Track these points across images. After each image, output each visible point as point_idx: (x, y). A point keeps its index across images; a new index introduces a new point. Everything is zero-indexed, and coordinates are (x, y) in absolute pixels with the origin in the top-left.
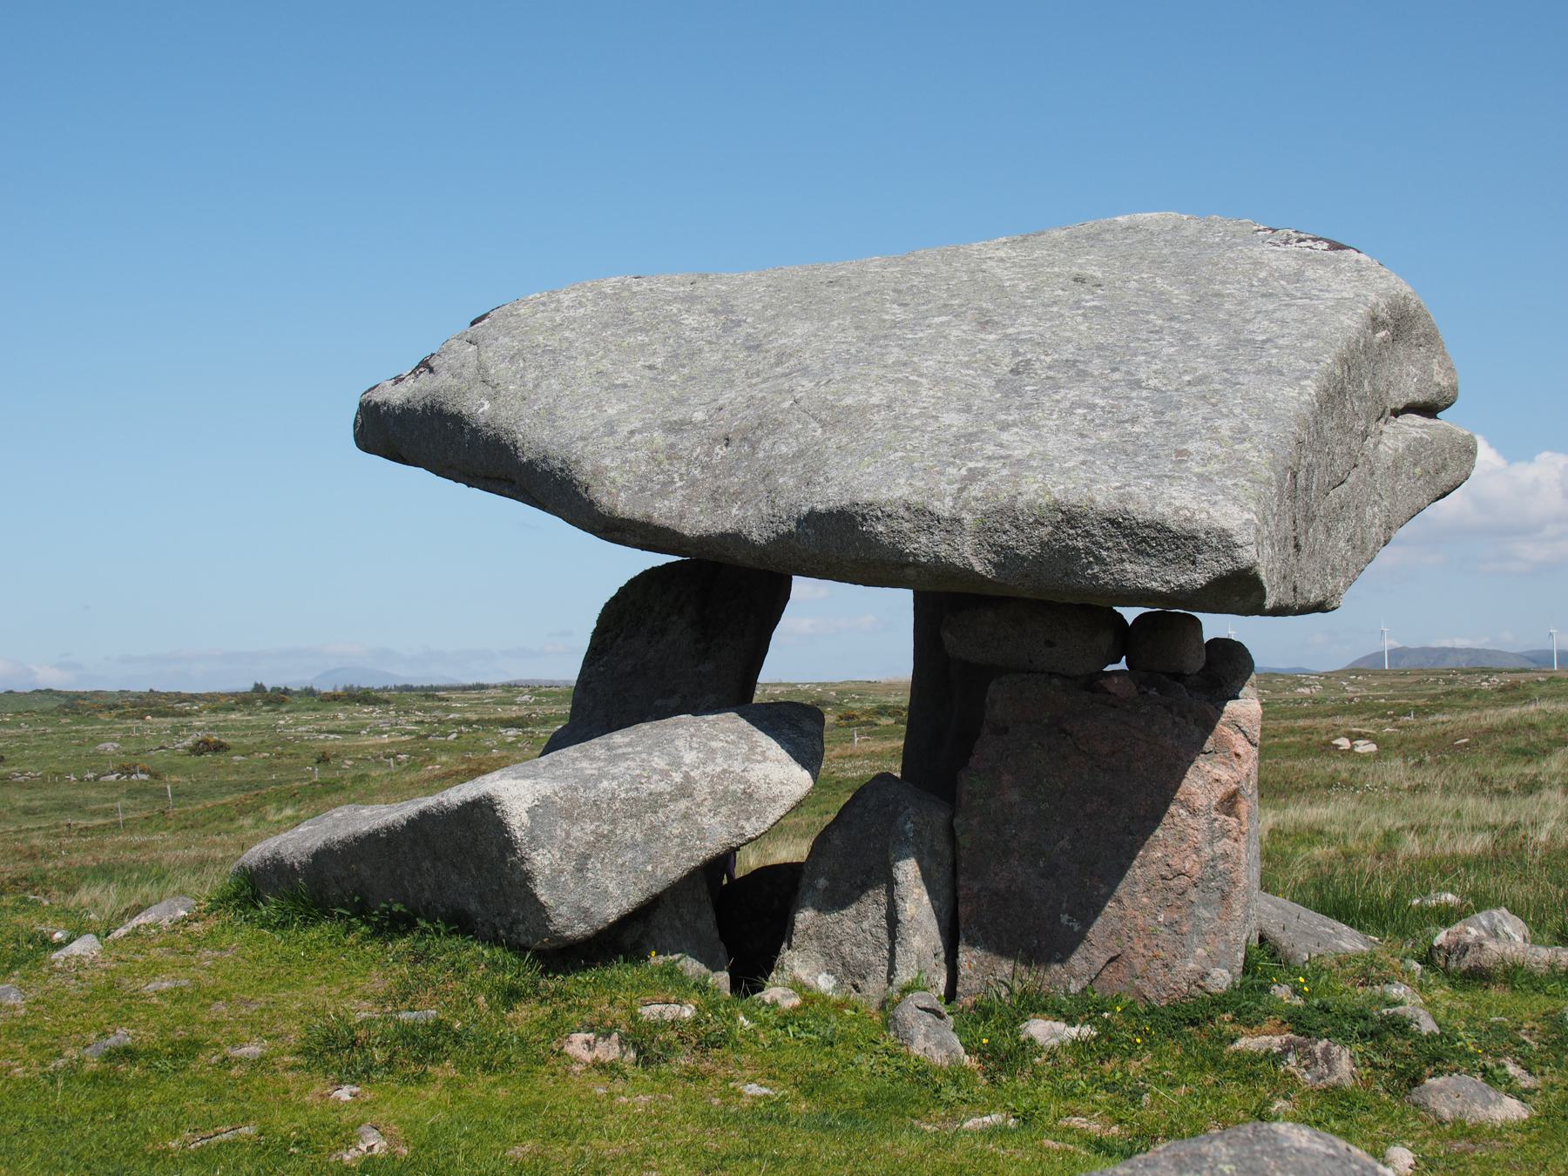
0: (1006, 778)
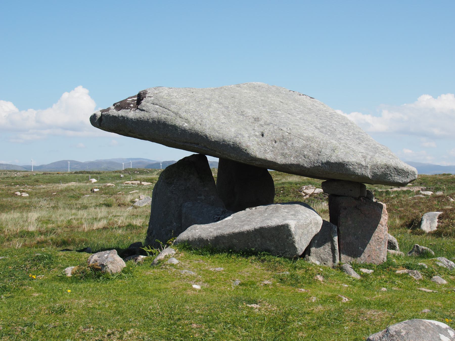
0: (349, 219)
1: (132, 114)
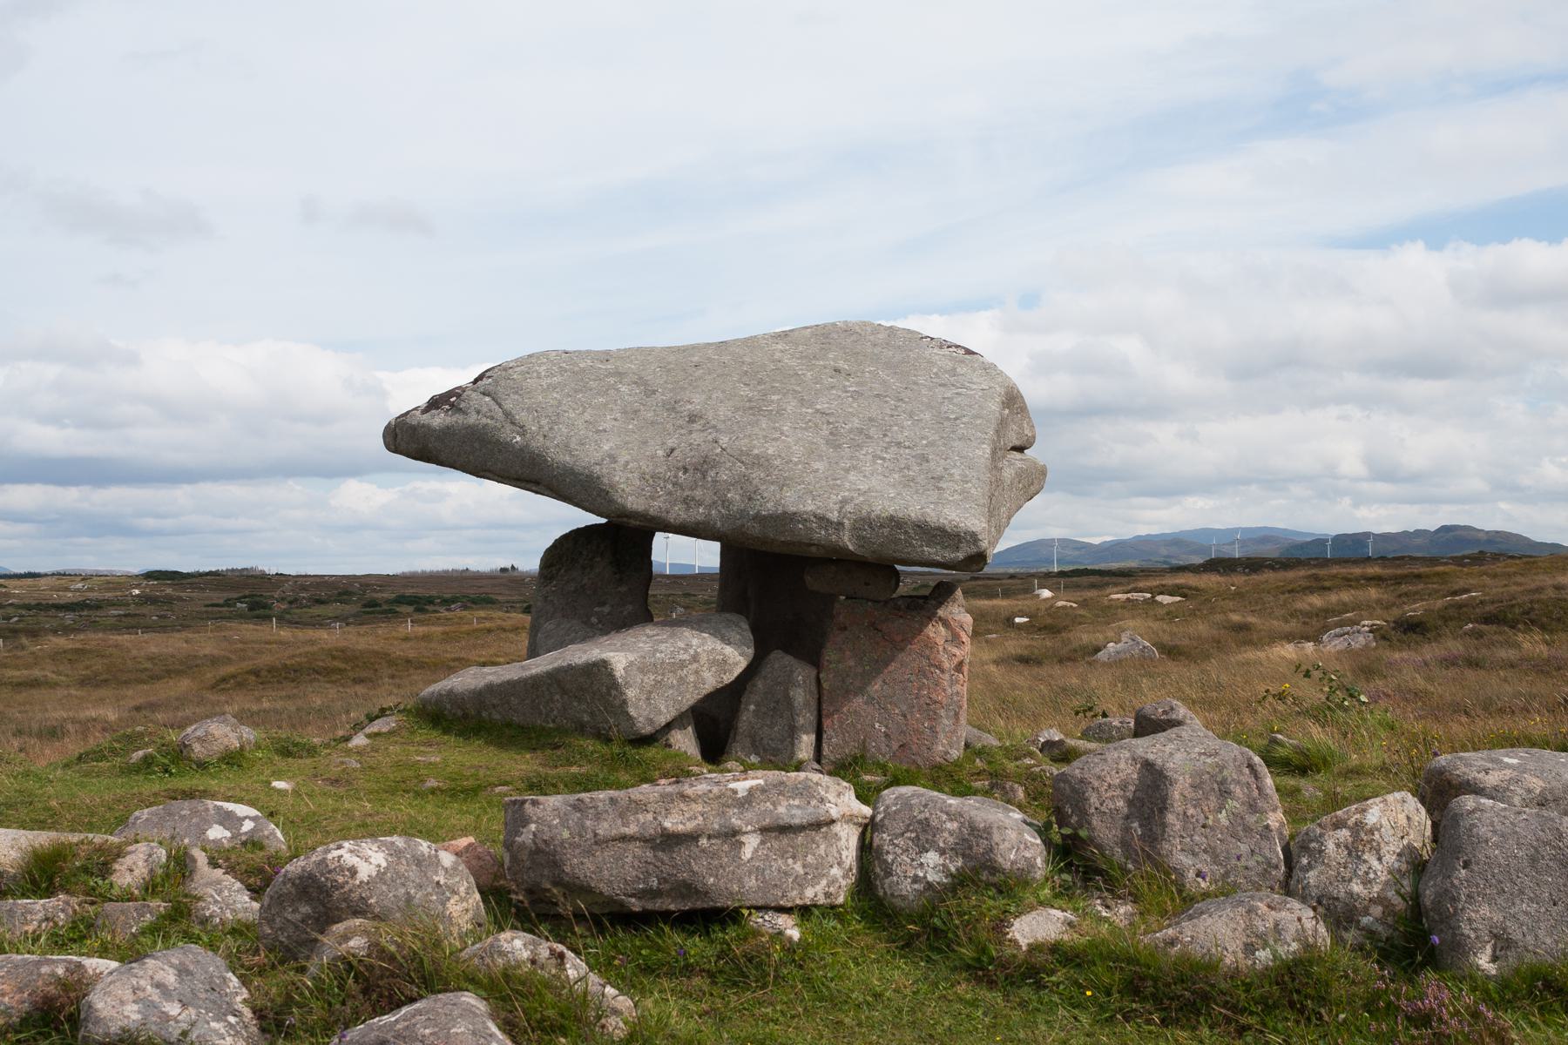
1: (438, 419)
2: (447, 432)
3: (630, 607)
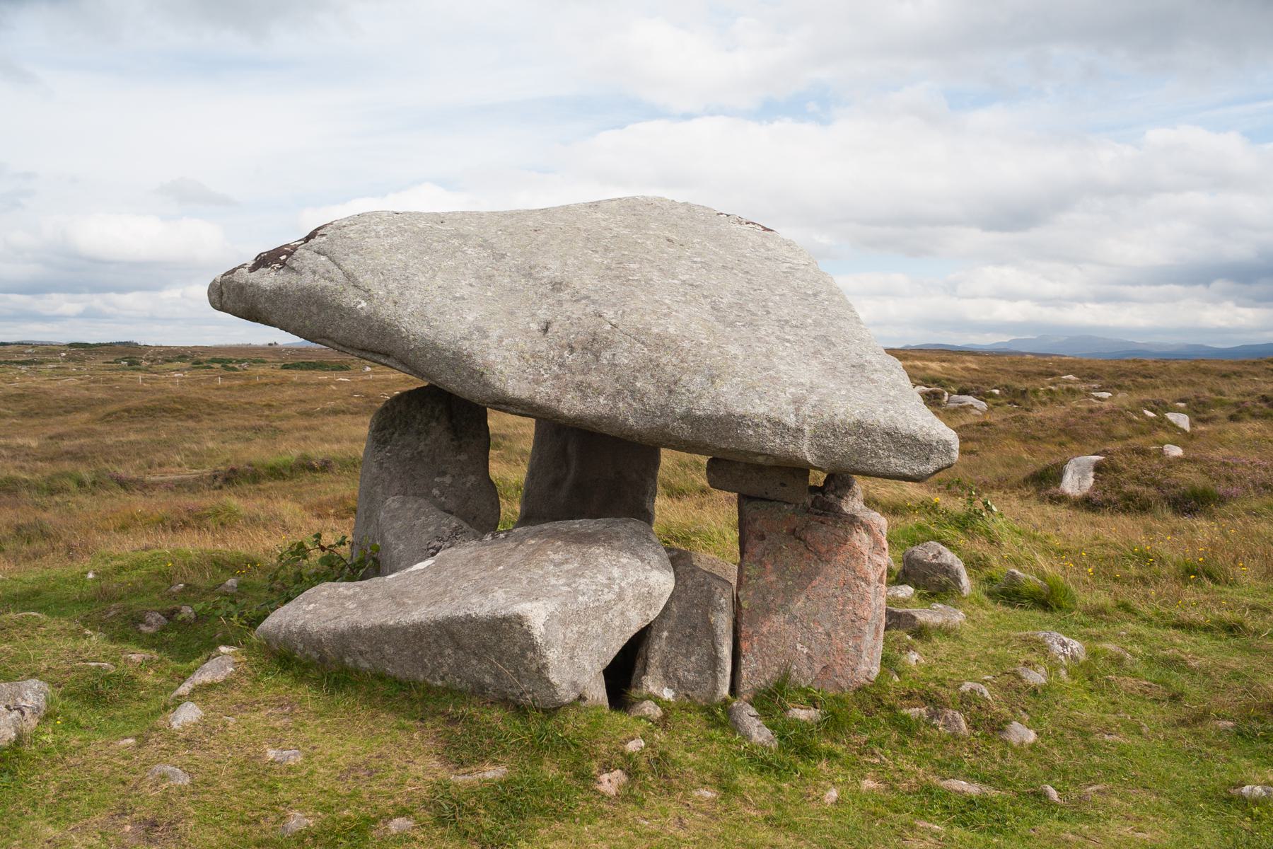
1: (268, 279)
2: (278, 294)
3: (473, 478)
